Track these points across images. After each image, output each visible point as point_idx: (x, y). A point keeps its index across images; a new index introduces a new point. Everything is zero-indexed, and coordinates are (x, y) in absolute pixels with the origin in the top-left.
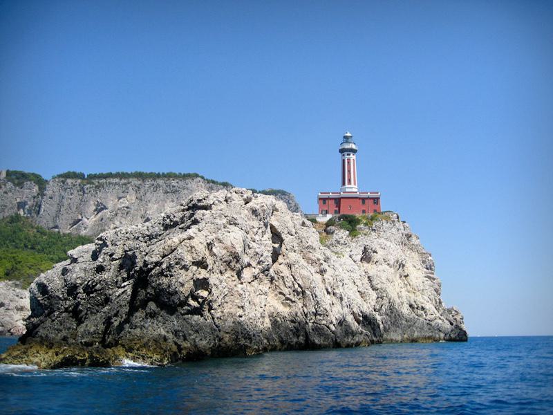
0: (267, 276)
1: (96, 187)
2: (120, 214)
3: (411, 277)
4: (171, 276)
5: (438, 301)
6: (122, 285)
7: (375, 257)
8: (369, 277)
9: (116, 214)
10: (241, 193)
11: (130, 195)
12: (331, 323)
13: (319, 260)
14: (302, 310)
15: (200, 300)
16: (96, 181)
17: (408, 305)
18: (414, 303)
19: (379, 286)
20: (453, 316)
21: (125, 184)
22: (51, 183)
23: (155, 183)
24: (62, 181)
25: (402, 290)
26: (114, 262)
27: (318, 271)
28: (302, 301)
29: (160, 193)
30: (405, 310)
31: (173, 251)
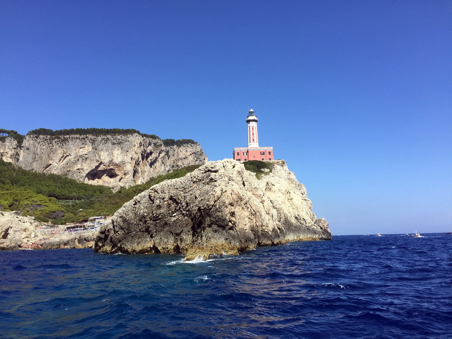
0: (246, 206)
1: (62, 141)
2: (81, 160)
3: (294, 200)
4: (222, 211)
5: (312, 214)
6: (173, 215)
7: (274, 188)
8: (271, 201)
9: (78, 160)
10: (231, 162)
11: (88, 146)
12: (270, 230)
13: (261, 195)
14: (255, 224)
15: (232, 222)
16: (62, 137)
17: (294, 218)
18: (298, 216)
19: (277, 207)
20: (322, 224)
21: (84, 138)
22: (27, 138)
23: (106, 138)
24: (36, 137)
25: (290, 208)
26: (165, 203)
27: (261, 201)
28: (255, 219)
29: (109, 144)
30: (293, 221)
31: (219, 199)
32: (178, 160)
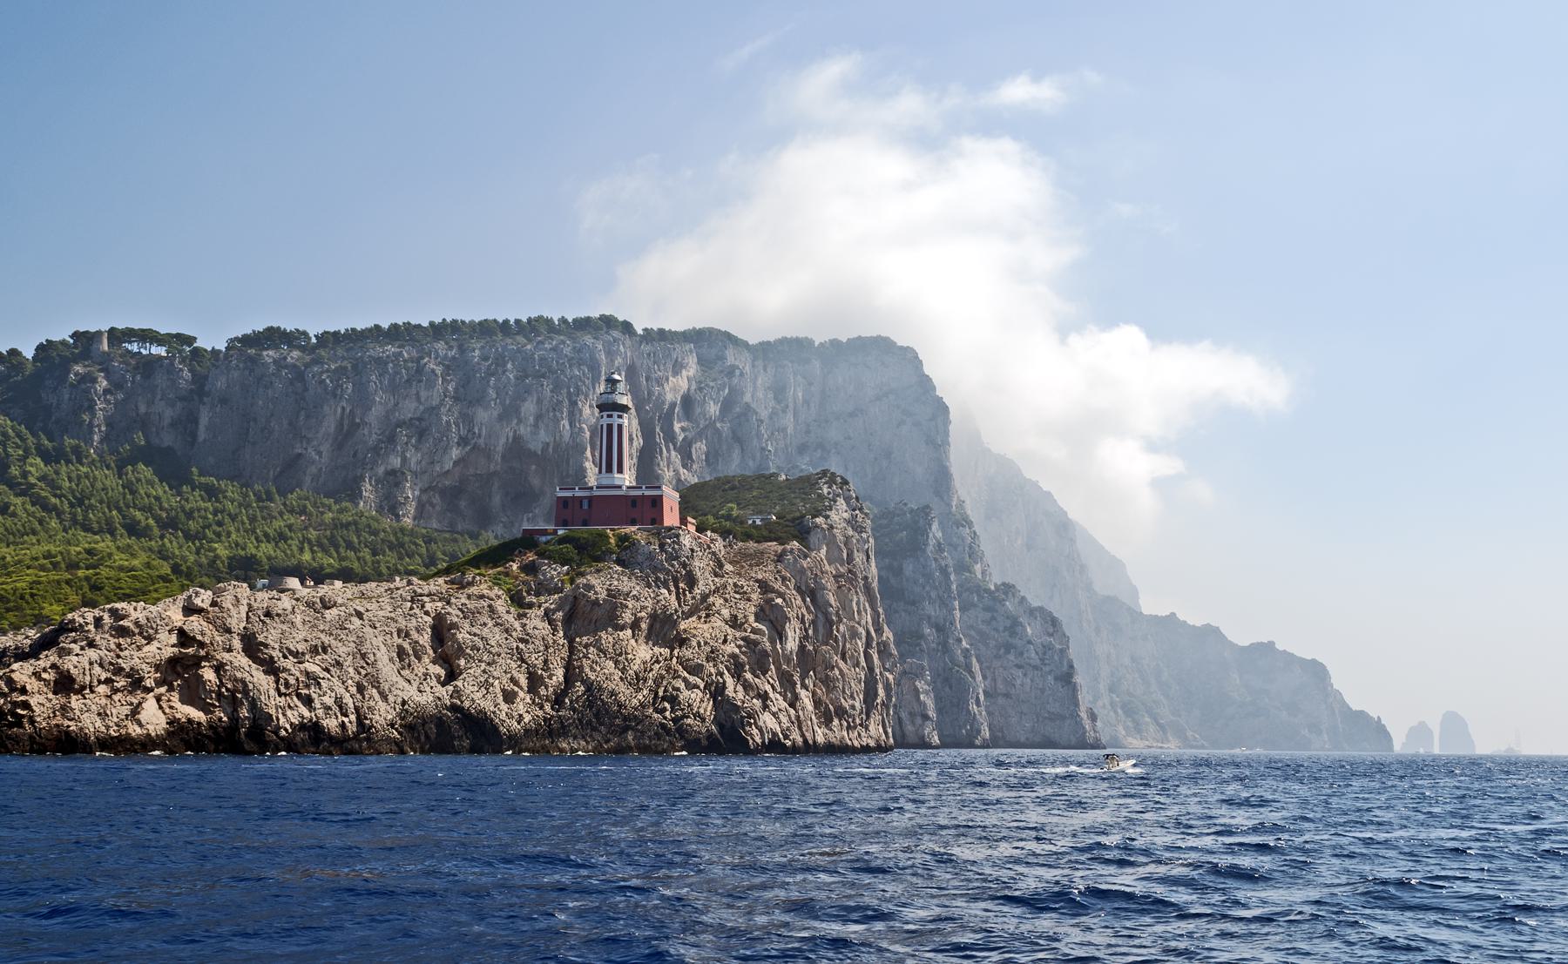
32: (827, 421)
